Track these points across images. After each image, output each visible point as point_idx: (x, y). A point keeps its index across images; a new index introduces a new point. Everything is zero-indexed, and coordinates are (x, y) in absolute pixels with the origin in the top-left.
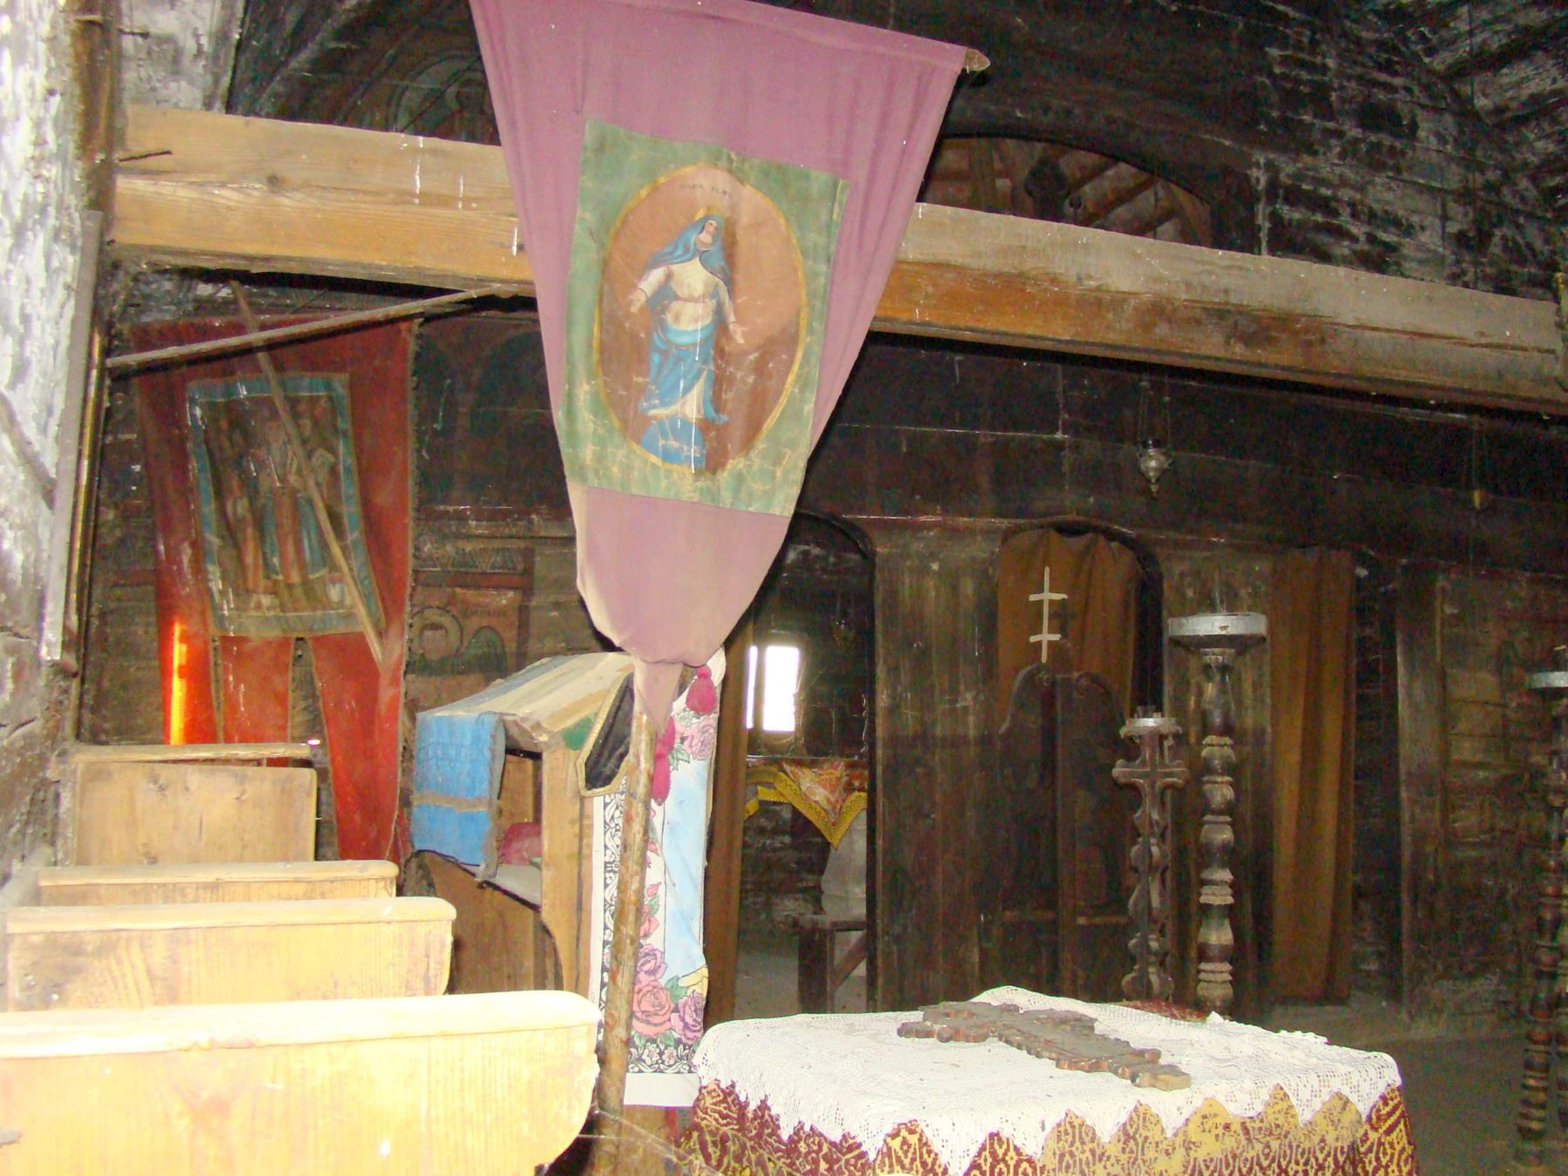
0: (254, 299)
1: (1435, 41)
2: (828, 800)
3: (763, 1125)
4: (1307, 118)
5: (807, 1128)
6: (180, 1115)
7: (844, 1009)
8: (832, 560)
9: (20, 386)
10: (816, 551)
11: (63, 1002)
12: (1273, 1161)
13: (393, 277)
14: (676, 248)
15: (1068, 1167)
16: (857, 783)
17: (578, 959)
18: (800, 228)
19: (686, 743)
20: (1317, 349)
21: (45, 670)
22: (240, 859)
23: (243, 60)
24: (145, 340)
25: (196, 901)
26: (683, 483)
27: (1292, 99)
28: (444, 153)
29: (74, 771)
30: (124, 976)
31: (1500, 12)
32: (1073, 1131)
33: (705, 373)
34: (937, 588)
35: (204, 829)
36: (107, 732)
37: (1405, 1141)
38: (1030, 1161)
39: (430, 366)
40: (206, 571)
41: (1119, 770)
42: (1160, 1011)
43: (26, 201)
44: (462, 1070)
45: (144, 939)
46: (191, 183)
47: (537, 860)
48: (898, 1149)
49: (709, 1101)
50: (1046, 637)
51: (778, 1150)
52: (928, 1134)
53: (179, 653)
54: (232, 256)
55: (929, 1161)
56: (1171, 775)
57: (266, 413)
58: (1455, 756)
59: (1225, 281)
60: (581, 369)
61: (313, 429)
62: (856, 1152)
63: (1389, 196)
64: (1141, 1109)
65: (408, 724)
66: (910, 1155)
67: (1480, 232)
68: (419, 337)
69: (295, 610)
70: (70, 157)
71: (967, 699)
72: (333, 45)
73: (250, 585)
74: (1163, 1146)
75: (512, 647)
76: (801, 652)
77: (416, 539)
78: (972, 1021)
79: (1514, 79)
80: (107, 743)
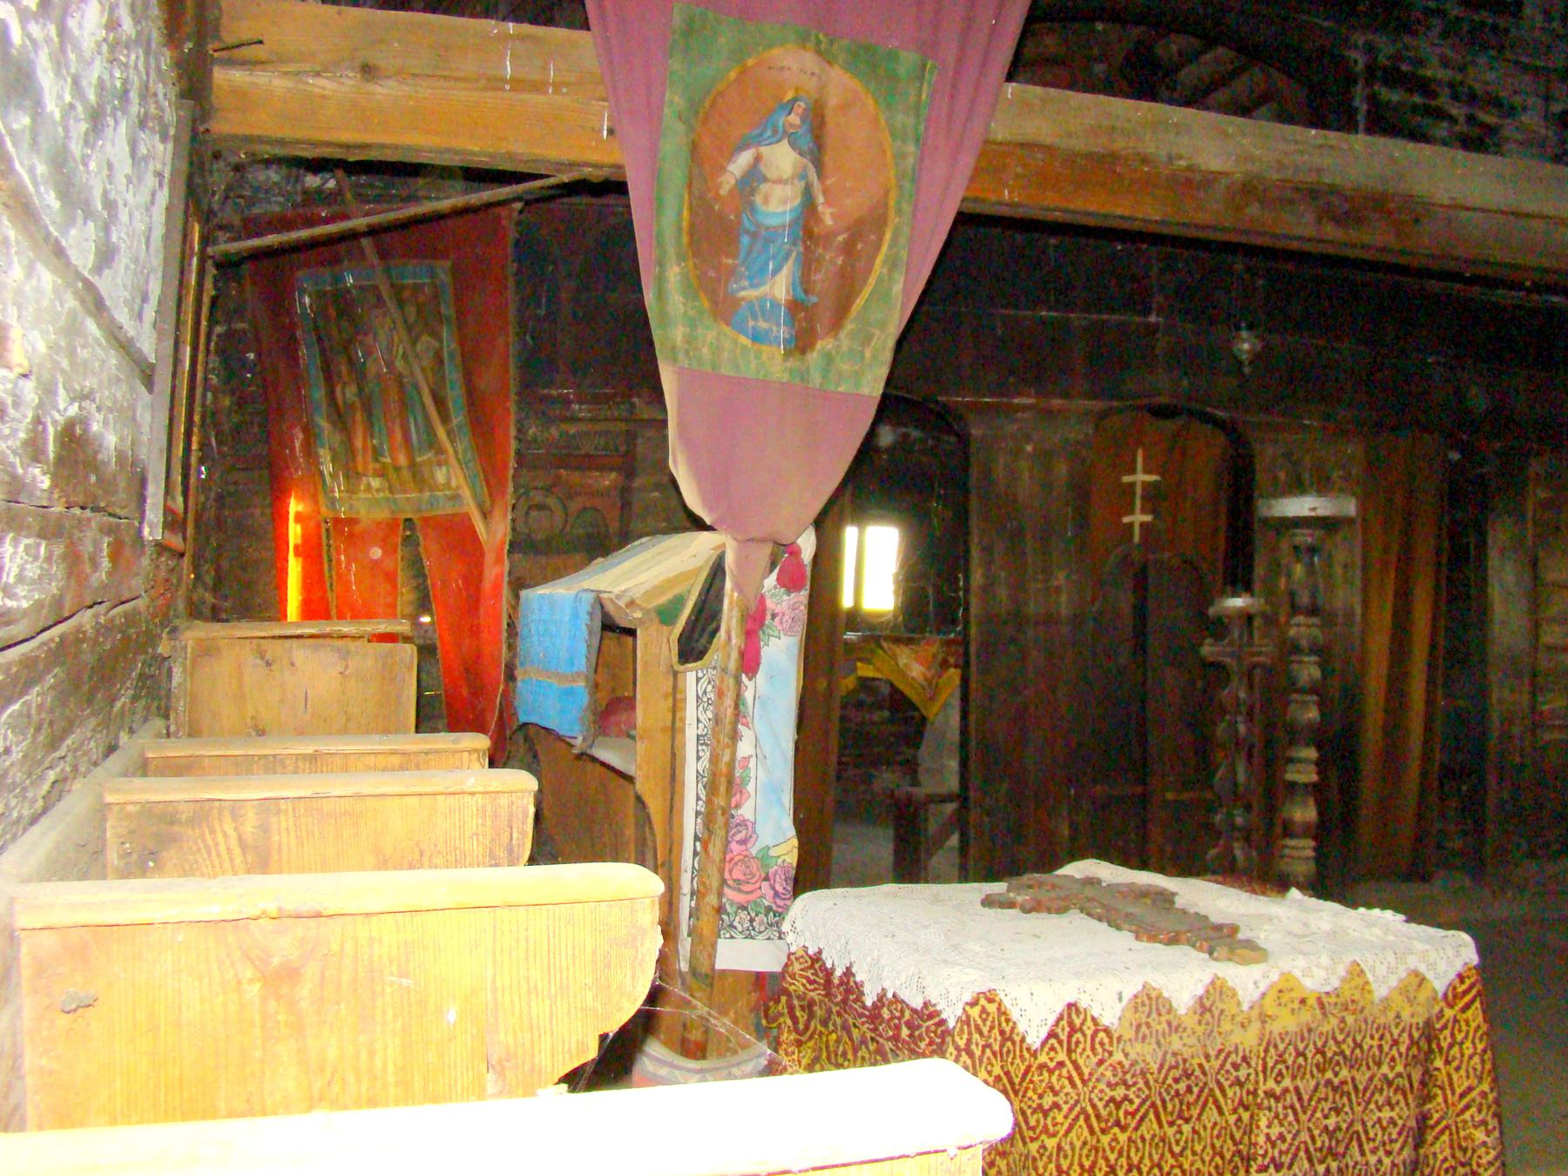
0: (362, 191)
2: (926, 679)
3: (849, 991)
5: (890, 995)
6: (251, 981)
7: (937, 879)
8: (930, 442)
9: (107, 271)
10: (915, 433)
11: (160, 869)
12: (1348, 1035)
13: (487, 163)
14: (764, 130)
15: (1144, 1038)
16: (952, 660)
17: (671, 829)
18: (888, 107)
19: (777, 619)
21: (149, 551)
24: (253, 227)
25: (295, 772)
26: (773, 363)
28: (536, 40)
29: (185, 647)
30: (217, 845)
32: (1150, 1003)
33: (794, 255)
34: (1031, 470)
35: (309, 702)
37: (1480, 1019)
38: (1106, 1031)
39: (530, 251)
40: (317, 456)
41: (1208, 649)
42: (1241, 887)
43: (101, 85)
44: (527, 940)
45: (236, 808)
46: (286, 73)
48: (977, 1018)
49: (797, 967)
50: (1139, 518)
51: (861, 1015)
52: (1007, 1002)
53: (294, 532)
54: (328, 144)
55: (1007, 1029)
57: (373, 300)
59: (1317, 161)
60: (671, 252)
62: (936, 1020)
64: (1218, 983)
66: (988, 1023)
69: (405, 492)
71: (1060, 578)
73: (360, 468)
74: (1239, 1019)
75: (614, 528)
76: (902, 537)
78: (1052, 894)
80: (227, 621)
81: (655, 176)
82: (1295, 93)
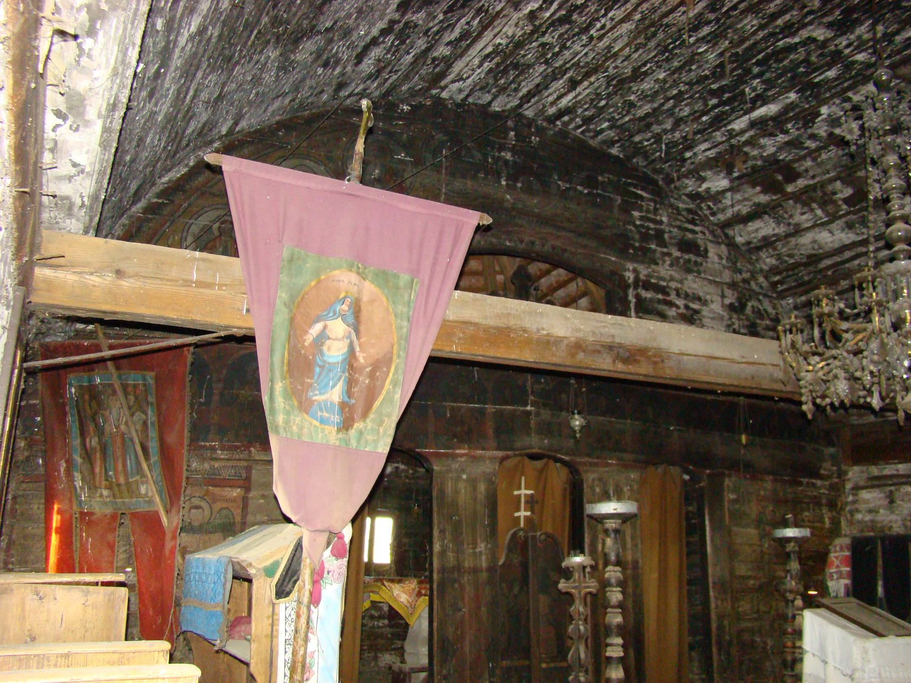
1: (715, 209)
4: (653, 247)
10: (402, 467)
16: (423, 592)
18: (394, 303)
20: (660, 365)
22: (83, 639)
23: (106, 207)
25: (55, 665)
26: (331, 435)
27: (645, 237)
28: (210, 261)
31: (746, 196)
34: (465, 488)
36: (13, 563)
39: (199, 368)
40: (73, 476)
41: (562, 585)
47: (249, 637)
53: (56, 520)
54: (94, 311)
56: (589, 587)
57: (110, 391)
58: (737, 573)
59: (613, 331)
60: (278, 374)
61: (135, 402)
63: (695, 286)
65: (181, 561)
67: (740, 302)
68: (193, 354)
69: (122, 498)
70: (9, 260)
71: (482, 547)
72: (155, 200)
73: (97, 484)
75: (238, 519)
77: (188, 461)
79: (754, 228)
81: (271, 338)
82: (599, 293)
